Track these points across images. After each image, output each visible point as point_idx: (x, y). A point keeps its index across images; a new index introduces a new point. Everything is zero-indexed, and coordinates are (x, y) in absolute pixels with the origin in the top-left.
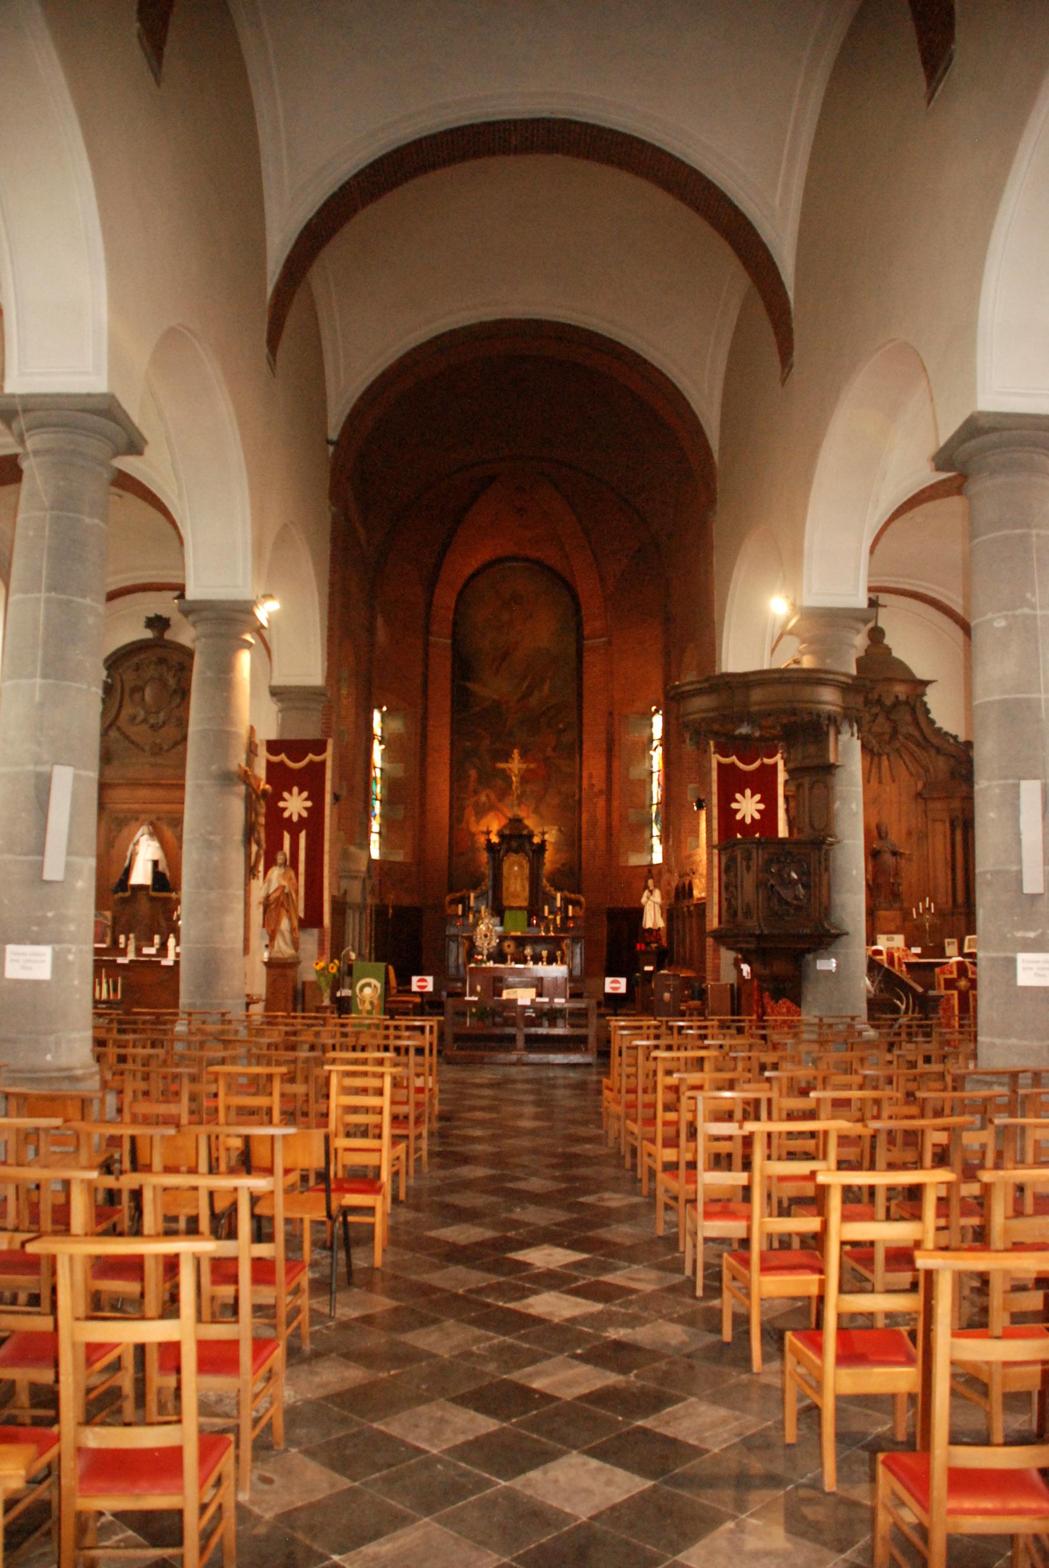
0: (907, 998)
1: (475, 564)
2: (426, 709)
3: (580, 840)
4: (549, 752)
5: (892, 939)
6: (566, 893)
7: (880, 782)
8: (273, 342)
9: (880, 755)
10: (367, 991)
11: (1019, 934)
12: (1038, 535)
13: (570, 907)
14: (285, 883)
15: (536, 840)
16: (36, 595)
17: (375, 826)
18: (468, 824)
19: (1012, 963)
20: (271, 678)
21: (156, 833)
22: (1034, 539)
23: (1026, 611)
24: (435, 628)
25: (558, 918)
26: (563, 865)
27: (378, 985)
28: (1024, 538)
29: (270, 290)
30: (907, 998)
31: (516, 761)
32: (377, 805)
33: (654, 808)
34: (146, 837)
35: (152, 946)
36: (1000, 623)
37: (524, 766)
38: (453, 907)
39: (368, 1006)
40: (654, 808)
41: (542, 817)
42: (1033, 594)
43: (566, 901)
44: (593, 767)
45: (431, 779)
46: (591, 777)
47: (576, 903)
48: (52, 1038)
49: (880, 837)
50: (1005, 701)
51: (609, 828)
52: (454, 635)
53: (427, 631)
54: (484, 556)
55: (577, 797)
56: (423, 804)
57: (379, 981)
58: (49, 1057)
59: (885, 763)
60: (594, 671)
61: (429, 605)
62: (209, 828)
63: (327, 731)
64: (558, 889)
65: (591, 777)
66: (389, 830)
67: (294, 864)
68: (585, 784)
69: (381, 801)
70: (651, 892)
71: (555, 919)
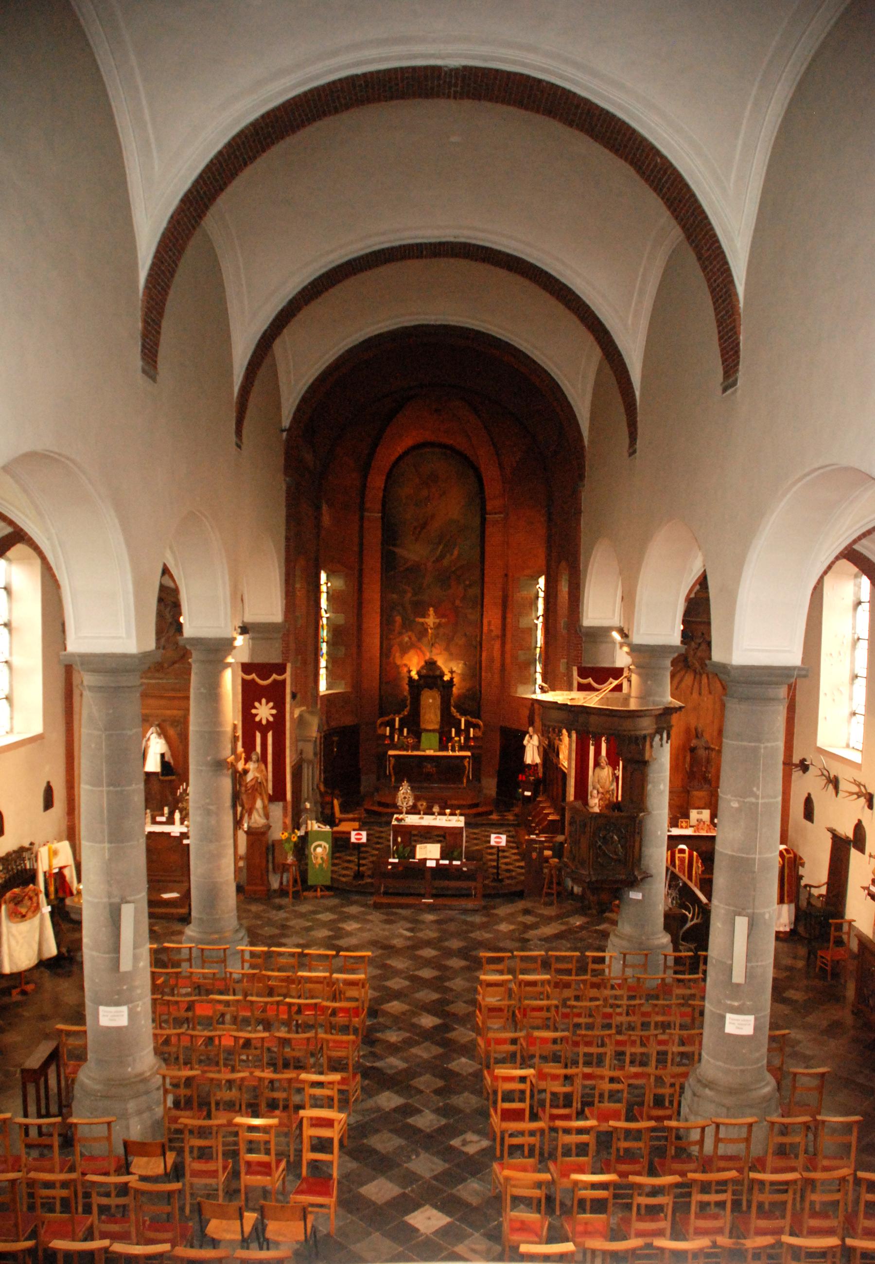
0: (694, 910)
1: (400, 450)
2: (361, 571)
3: (481, 673)
4: (458, 602)
5: (701, 813)
6: (469, 718)
7: (700, 694)
8: (239, 432)
9: (701, 675)
10: (319, 850)
11: (729, 1002)
12: (766, 748)
13: (472, 730)
14: (258, 775)
15: (446, 678)
16: (100, 789)
17: (323, 663)
18: (394, 659)
19: (722, 1018)
20: (243, 617)
21: (163, 733)
22: (762, 751)
23: (753, 800)
24: (368, 505)
25: (462, 738)
26: (468, 690)
27: (327, 846)
28: (755, 750)
29: (236, 389)
30: (694, 910)
31: (432, 617)
32: (324, 647)
33: (538, 650)
34: (154, 735)
35: (162, 815)
36: (735, 805)
37: (437, 621)
38: (382, 728)
39: (320, 861)
40: (538, 650)
41: (451, 654)
42: (758, 789)
43: (468, 724)
44: (492, 618)
45: (365, 626)
46: (489, 623)
47: (475, 726)
48: (130, 1058)
49: (697, 736)
50: (732, 857)
51: (503, 665)
52: (384, 510)
53: (362, 508)
54: (408, 442)
55: (478, 639)
56: (359, 646)
57: (327, 842)
58: (130, 1069)
59: (705, 680)
60: (494, 536)
61: (364, 486)
62: (208, 801)
63: (285, 652)
64: (464, 713)
65: (489, 623)
66: (333, 666)
67: (263, 759)
68: (485, 628)
69: (327, 642)
70: (531, 737)
71: (460, 740)
